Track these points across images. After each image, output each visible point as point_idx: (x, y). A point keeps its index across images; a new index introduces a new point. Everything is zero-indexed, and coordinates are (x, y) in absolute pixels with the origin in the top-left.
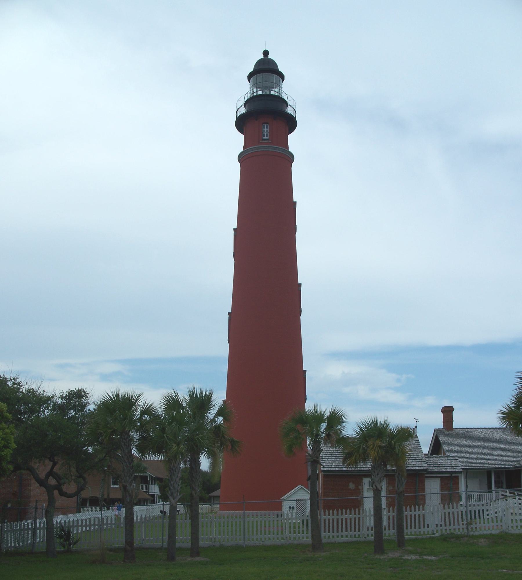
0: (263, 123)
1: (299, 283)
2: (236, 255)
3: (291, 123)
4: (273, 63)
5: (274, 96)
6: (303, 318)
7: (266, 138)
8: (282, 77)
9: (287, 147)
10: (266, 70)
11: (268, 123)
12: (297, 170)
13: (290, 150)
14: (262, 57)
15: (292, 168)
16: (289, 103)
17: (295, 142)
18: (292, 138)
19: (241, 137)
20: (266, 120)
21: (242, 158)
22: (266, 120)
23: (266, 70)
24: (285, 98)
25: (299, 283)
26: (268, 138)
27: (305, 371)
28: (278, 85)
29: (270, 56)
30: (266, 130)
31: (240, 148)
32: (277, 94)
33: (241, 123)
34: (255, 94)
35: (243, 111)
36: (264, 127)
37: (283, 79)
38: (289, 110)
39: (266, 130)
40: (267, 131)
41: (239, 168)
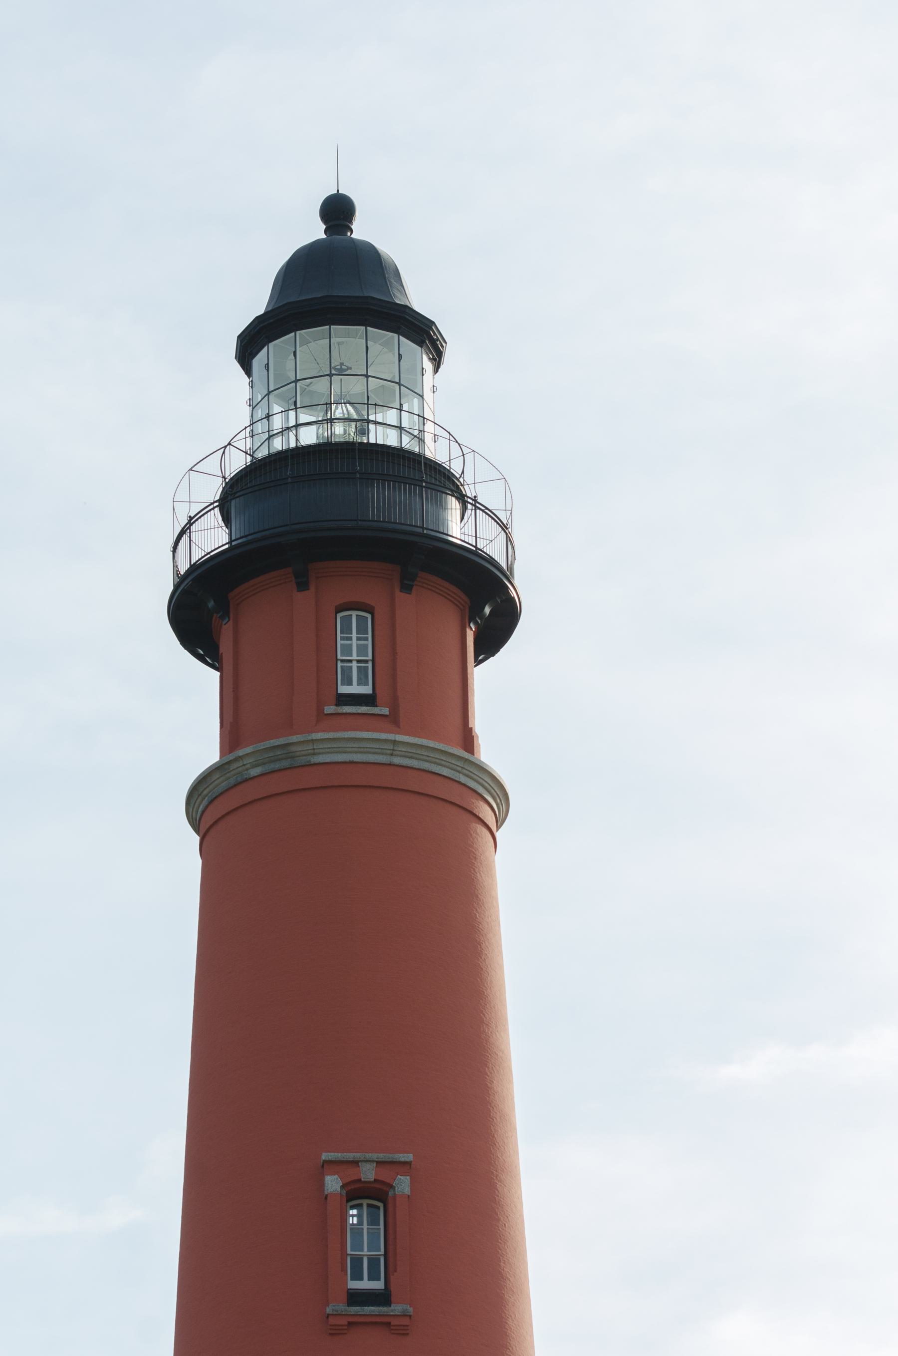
0: (339, 610)
2: (499, 651)
4: (371, 265)
7: (355, 689)
9: (468, 740)
10: (336, 290)
11: (370, 610)
14: (317, 231)
17: (509, 704)
18: (485, 677)
19: (199, 687)
20: (338, 581)
21: (209, 805)
22: (338, 581)
23: (336, 290)
26: (367, 690)
31: (206, 751)
32: (407, 443)
33: (202, 609)
35: (213, 536)
36: (347, 629)
37: (437, 359)
40: (361, 650)
41: (196, 863)
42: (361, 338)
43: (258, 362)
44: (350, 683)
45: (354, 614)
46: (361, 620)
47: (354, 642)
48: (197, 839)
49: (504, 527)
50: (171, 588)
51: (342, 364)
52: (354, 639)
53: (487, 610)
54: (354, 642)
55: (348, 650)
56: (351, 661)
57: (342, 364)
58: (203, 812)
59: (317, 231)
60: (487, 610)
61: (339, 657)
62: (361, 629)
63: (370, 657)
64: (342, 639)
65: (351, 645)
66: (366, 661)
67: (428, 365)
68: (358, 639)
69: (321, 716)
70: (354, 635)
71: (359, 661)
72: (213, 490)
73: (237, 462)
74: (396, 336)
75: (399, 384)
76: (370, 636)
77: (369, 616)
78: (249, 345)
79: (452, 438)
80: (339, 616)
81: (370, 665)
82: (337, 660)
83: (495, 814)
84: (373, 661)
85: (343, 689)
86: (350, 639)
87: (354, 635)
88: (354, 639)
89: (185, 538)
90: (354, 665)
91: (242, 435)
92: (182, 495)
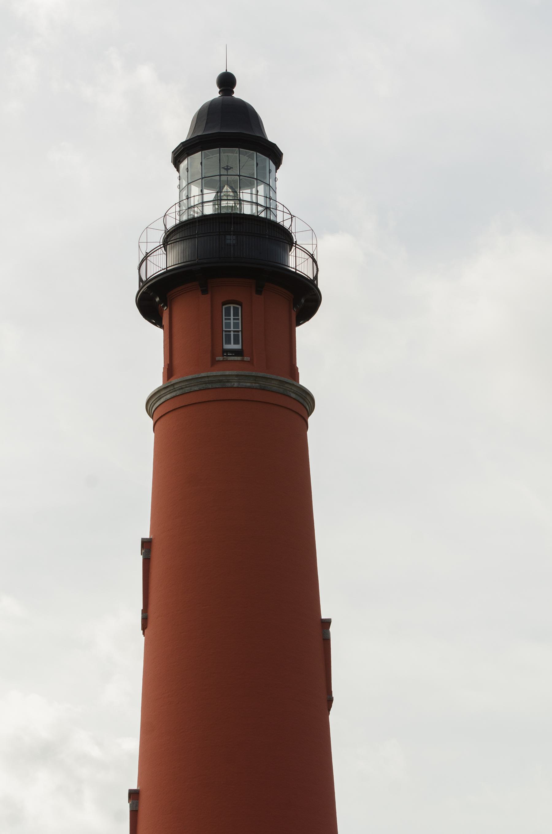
0: (224, 304)
1: (324, 616)
3: (304, 297)
5: (253, 219)
6: (336, 718)
7: (232, 346)
8: (275, 155)
9: (294, 373)
10: (229, 131)
11: (240, 304)
12: (324, 440)
13: (303, 381)
14: (214, 93)
15: (309, 433)
16: (298, 238)
18: (303, 332)
20: (231, 288)
21: (155, 404)
22: (231, 288)
23: (229, 131)
24: (287, 225)
25: (324, 616)
26: (238, 347)
27: (327, 623)
28: (262, 178)
29: (238, 93)
30: (232, 323)
34: (185, 218)
35: (159, 264)
38: (297, 262)
39: (232, 323)
40: (236, 325)
42: (237, 153)
43: (184, 165)
44: (229, 343)
45: (232, 306)
46: (236, 310)
47: (232, 321)
48: (151, 422)
49: (312, 256)
50: (138, 289)
51: (227, 166)
52: (232, 319)
53: (303, 301)
54: (232, 321)
55: (228, 325)
56: (230, 331)
57: (227, 166)
58: (154, 411)
59: (214, 93)
60: (303, 301)
61: (224, 329)
62: (236, 314)
63: (240, 329)
64: (226, 319)
65: (230, 323)
66: (238, 331)
67: (273, 167)
68: (234, 319)
69: (214, 362)
70: (232, 317)
71: (234, 331)
72: (158, 236)
73: (171, 223)
74: (255, 153)
75: (257, 179)
76: (240, 317)
77: (240, 307)
78: (180, 155)
79: (285, 210)
80: (224, 307)
81: (240, 333)
82: (223, 331)
83: (307, 410)
84: (242, 331)
85: (226, 347)
86: (230, 319)
87: (232, 317)
88: (232, 319)
89: (145, 262)
90: (232, 333)
91: (173, 210)
92: (143, 239)
